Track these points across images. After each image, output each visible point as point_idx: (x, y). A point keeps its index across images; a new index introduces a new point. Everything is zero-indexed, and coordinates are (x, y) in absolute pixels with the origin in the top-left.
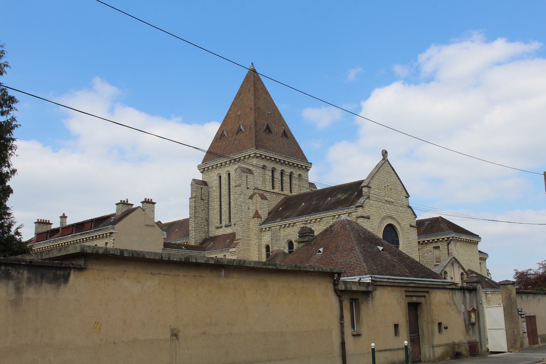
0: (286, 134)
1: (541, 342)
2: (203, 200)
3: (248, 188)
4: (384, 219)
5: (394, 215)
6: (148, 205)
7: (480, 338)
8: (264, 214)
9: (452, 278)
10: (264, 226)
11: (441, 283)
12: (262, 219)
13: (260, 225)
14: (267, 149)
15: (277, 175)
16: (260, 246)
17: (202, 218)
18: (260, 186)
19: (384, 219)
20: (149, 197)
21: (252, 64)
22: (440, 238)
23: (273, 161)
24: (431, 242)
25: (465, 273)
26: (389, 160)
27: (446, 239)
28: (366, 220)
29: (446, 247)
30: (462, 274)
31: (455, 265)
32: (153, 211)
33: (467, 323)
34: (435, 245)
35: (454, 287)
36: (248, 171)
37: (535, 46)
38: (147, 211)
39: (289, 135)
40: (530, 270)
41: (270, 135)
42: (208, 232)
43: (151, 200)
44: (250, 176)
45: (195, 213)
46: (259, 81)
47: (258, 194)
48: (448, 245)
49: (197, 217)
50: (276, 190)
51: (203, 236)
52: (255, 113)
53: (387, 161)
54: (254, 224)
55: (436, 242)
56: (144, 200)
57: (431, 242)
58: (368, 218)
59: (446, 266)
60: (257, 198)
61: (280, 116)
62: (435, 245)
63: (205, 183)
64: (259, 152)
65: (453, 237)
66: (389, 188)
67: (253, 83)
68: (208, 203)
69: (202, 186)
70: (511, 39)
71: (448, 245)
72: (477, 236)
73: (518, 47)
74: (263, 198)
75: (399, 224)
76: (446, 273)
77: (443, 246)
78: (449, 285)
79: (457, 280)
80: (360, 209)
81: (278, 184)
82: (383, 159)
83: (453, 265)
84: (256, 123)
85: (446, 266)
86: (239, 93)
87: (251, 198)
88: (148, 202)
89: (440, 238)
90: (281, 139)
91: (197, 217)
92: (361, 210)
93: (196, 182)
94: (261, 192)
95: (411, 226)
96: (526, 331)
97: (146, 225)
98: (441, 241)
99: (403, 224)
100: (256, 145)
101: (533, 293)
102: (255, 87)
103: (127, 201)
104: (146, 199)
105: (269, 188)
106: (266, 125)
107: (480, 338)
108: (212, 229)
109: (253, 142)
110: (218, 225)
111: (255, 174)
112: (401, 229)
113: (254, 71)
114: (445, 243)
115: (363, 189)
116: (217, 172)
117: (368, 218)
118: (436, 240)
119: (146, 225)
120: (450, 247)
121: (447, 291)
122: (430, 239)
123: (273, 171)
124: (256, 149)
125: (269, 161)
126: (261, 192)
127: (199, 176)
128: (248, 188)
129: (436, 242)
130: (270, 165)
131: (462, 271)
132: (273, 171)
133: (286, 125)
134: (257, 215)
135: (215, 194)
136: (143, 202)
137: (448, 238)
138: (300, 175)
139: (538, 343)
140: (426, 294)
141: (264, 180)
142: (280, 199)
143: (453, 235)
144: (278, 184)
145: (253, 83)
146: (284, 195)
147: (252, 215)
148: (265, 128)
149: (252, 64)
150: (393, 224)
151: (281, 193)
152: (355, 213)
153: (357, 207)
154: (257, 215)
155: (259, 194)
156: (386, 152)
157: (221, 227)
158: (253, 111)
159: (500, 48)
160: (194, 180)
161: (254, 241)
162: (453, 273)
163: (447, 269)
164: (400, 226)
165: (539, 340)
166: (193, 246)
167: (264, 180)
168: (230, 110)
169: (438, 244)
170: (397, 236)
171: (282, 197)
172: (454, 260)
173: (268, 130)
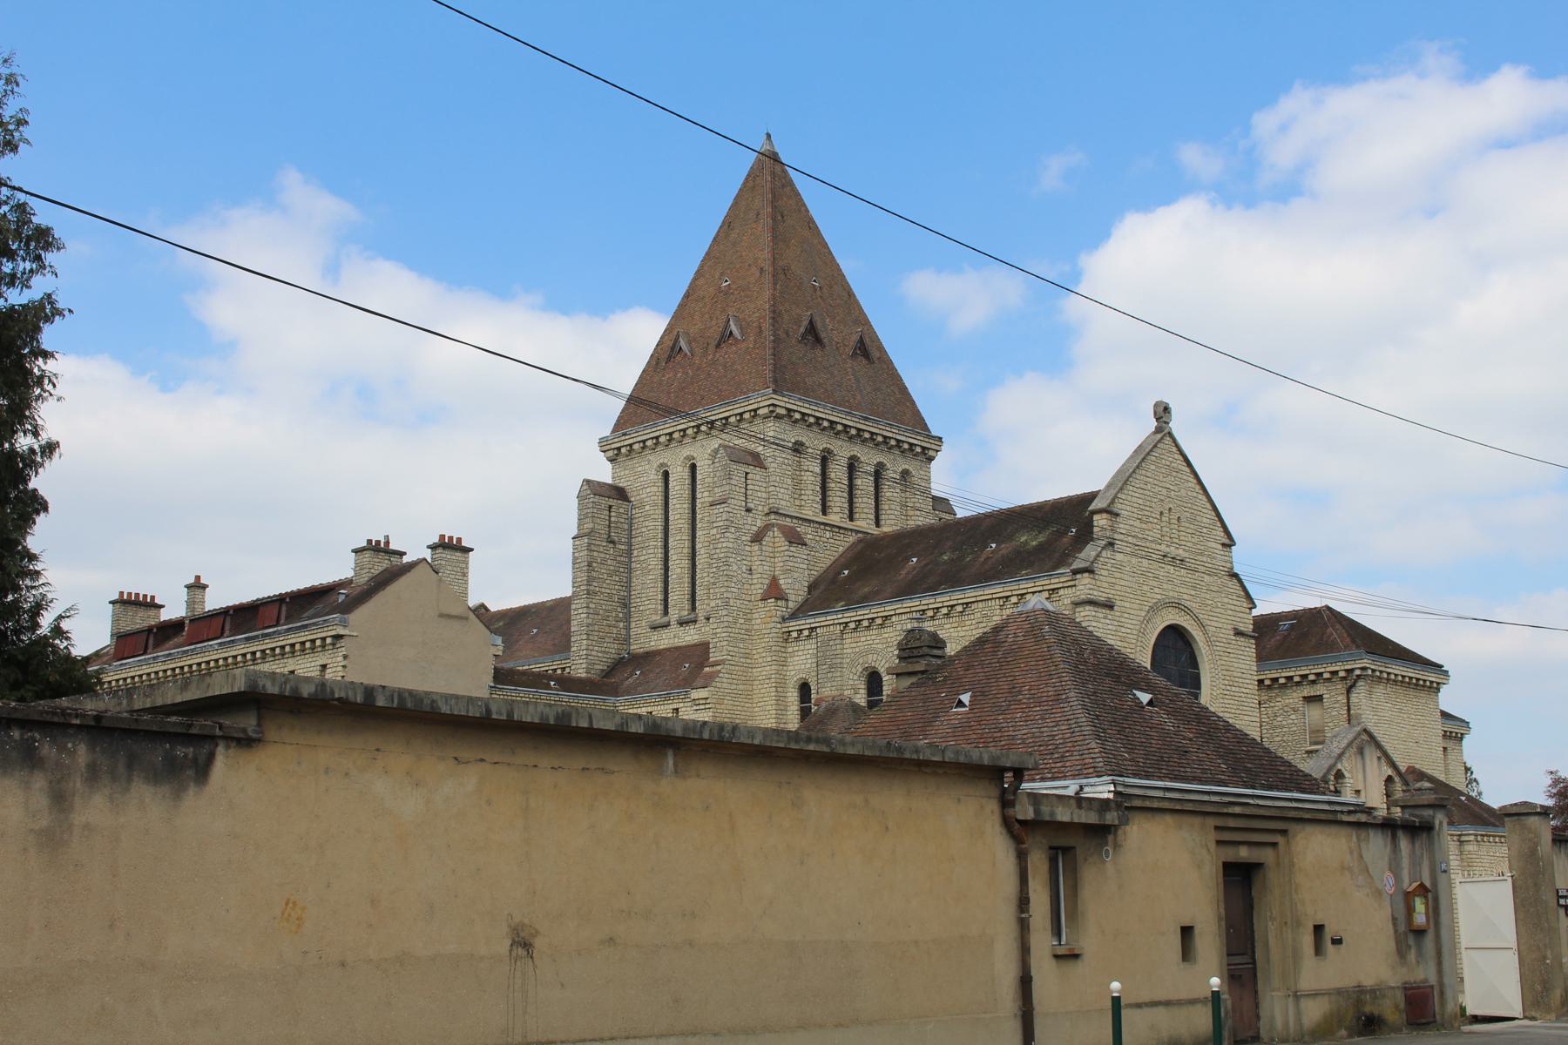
0: (867, 350)
2: (613, 542)
3: (748, 510)
4: (1155, 609)
6: (448, 555)
9: (1358, 792)
10: (794, 625)
11: (1327, 807)
12: (791, 604)
14: (805, 392)
15: (838, 472)
16: (780, 685)
18: (785, 505)
19: (1155, 609)
20: (453, 532)
21: (769, 136)
22: (1325, 669)
23: (824, 429)
24: (1298, 684)
25: (1397, 779)
27: (1342, 674)
29: (1343, 699)
30: (1389, 780)
32: (465, 575)
35: (1363, 818)
36: (749, 459)
39: (875, 354)
41: (818, 352)
42: (627, 639)
43: (459, 540)
44: (756, 474)
45: (589, 582)
48: (1349, 691)
49: (595, 593)
50: (834, 518)
51: (612, 650)
53: (1170, 434)
54: (766, 617)
55: (1313, 682)
57: (1298, 684)
59: (1340, 756)
60: (776, 539)
64: (784, 402)
66: (1174, 517)
67: (771, 192)
68: (630, 552)
69: (612, 502)
71: (1349, 691)
72: (1437, 667)
74: (795, 539)
75: (1202, 626)
76: (1339, 775)
77: (1333, 695)
78: (1350, 812)
79: (1375, 798)
80: (1085, 579)
81: (838, 500)
82: (1158, 430)
83: (1361, 751)
84: (776, 316)
85: (1340, 756)
86: (728, 225)
87: (757, 538)
88: (450, 547)
89: (1325, 669)
91: (595, 593)
92: (1086, 581)
93: (592, 489)
95: (1238, 633)
97: (441, 616)
99: (1212, 625)
100: (775, 381)
102: (774, 207)
103: (387, 543)
105: (812, 510)
106: (805, 323)
109: (768, 371)
110: (658, 618)
112: (1209, 642)
113: (774, 158)
114: (1341, 687)
119: (441, 616)
120: (1354, 698)
121: (1344, 831)
124: (775, 392)
125: (815, 428)
127: (604, 473)
128: (748, 510)
129: (1313, 682)
130: (816, 442)
133: (867, 323)
134: (774, 591)
135: (649, 526)
136: (433, 547)
138: (905, 474)
140: (1279, 839)
141: (798, 485)
143: (1365, 663)
144: (838, 500)
145: (771, 192)
146: (857, 532)
148: (802, 330)
149: (769, 136)
150: (1189, 628)
151: (849, 525)
153: (1075, 572)
154: (774, 591)
156: (1166, 409)
157: (667, 625)
158: (768, 278)
159: (1509, 95)
160: (588, 482)
161: (764, 669)
162: (1360, 776)
163: (1344, 766)
164: (1205, 633)
166: (580, 680)
167: (798, 485)
170: (1194, 663)
171: (852, 538)
172: (1365, 737)
173: (813, 334)
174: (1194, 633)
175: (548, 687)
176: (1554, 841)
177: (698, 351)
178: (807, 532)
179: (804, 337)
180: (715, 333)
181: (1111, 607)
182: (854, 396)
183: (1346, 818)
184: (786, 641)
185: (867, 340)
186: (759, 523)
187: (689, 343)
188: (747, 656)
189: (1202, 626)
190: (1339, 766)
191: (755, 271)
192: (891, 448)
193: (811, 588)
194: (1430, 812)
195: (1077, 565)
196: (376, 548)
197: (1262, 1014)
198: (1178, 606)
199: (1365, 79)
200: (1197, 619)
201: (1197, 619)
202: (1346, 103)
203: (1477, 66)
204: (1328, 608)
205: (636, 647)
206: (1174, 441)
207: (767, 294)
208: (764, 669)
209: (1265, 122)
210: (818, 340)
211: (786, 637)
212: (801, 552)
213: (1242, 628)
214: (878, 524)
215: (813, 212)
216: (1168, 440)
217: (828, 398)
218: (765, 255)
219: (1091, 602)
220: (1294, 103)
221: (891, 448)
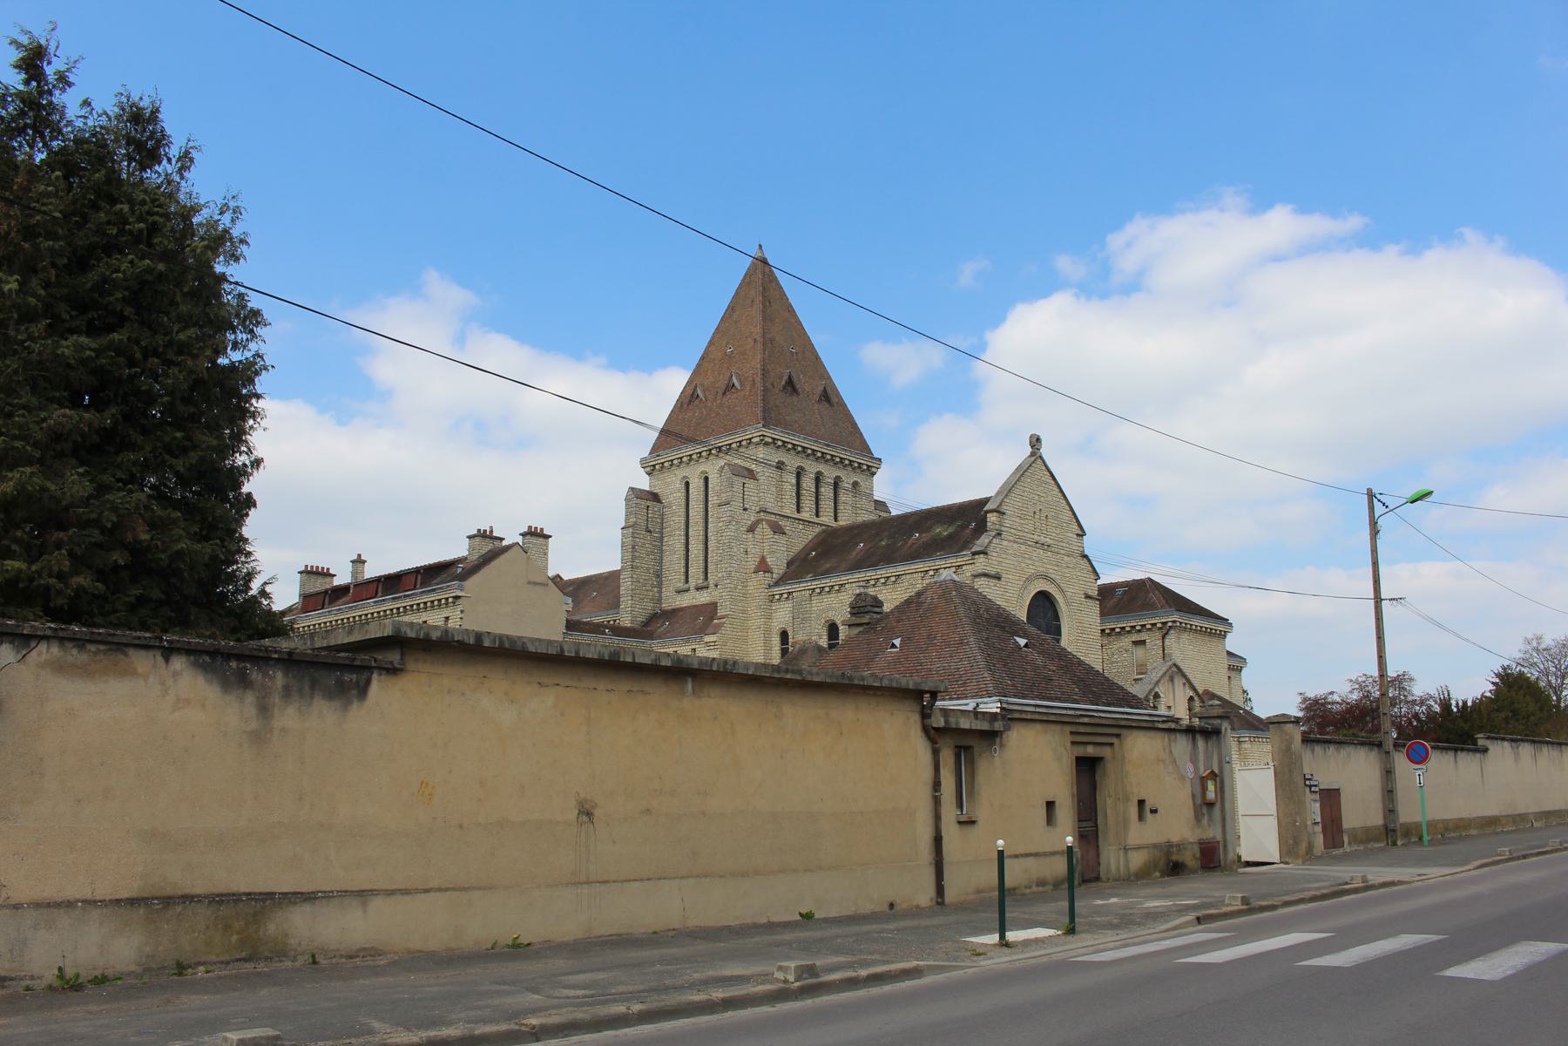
0: (829, 396)
4: (1030, 579)
6: (534, 540)
7: (1224, 832)
10: (777, 590)
15: (808, 483)
16: (767, 632)
18: (771, 507)
19: (1030, 579)
20: (537, 524)
22: (1148, 622)
29: (1159, 643)
30: (1191, 699)
33: (1199, 801)
34: (1135, 637)
35: (1173, 726)
38: (532, 552)
39: (834, 399)
41: (795, 398)
42: (660, 599)
44: (750, 484)
45: (634, 558)
50: (805, 515)
51: (649, 607)
59: (1157, 683)
60: (764, 529)
61: (817, 358)
62: (1135, 637)
64: (770, 433)
67: (761, 285)
68: (662, 538)
74: (778, 530)
77: (1153, 639)
79: (1181, 712)
80: (981, 559)
81: (808, 502)
82: (1032, 454)
83: (1172, 679)
84: (765, 373)
85: (1157, 683)
86: (731, 309)
87: (751, 529)
88: (535, 534)
89: (1148, 622)
93: (635, 493)
95: (1088, 597)
99: (1069, 590)
105: (790, 510)
107: (1224, 832)
110: (681, 585)
112: (1067, 603)
114: (1158, 635)
116: (681, 473)
117: (998, 577)
121: (1159, 735)
122: (1127, 625)
127: (644, 482)
130: (793, 462)
134: (763, 567)
135: (675, 520)
137: (1164, 624)
138: (855, 484)
140: (1114, 740)
143: (1175, 618)
144: (808, 502)
145: (761, 285)
147: (752, 566)
151: (797, 516)
153: (974, 554)
154: (763, 567)
155: (770, 523)
156: (1038, 440)
161: (756, 621)
163: (1160, 689)
165: (1346, 839)
166: (627, 629)
167: (780, 494)
168: (711, 343)
170: (1057, 618)
171: (818, 530)
181: (999, 579)
193: (789, 564)
195: (975, 549)
196: (484, 535)
198: (1046, 578)
200: (1059, 587)
201: (1059, 587)
208: (756, 621)
210: (795, 390)
211: (771, 599)
219: (985, 575)
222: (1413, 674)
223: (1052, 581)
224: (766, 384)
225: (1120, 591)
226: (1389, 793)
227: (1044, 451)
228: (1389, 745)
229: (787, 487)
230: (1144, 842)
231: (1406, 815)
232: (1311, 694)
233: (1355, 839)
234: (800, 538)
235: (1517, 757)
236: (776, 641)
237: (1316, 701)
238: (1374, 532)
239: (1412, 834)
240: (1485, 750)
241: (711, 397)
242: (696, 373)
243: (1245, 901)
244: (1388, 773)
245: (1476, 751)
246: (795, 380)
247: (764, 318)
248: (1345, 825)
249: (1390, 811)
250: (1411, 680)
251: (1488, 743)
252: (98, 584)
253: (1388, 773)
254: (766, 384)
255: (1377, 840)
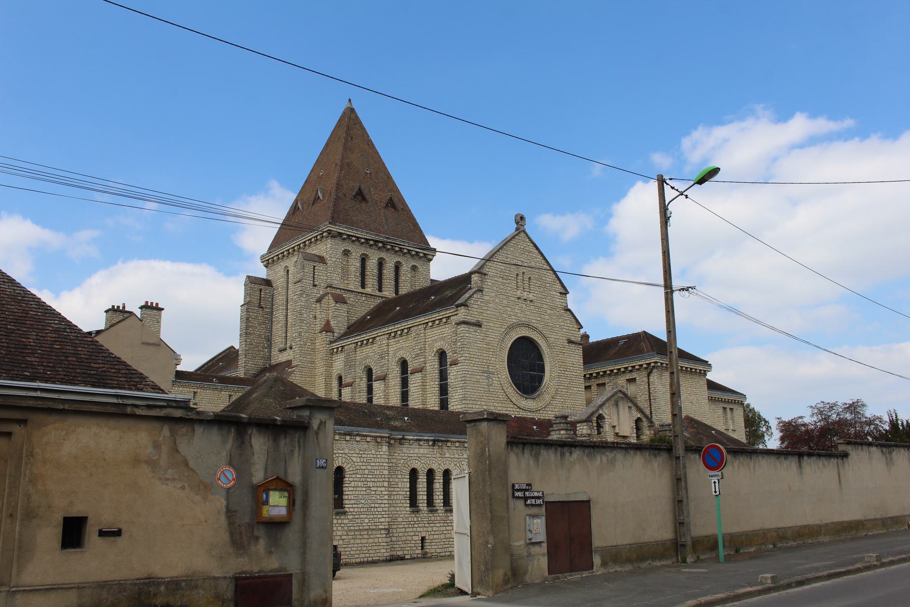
0: (395, 203)
1: (604, 564)
2: (262, 308)
3: (315, 286)
4: (512, 327)
5: (534, 322)
6: (148, 312)
7: (304, 561)
8: (339, 327)
9: (614, 427)
10: (335, 345)
11: (114, 401)
12: (336, 335)
13: (331, 342)
14: (351, 224)
15: (372, 264)
16: (328, 377)
17: (260, 336)
18: (336, 283)
19: (512, 327)
20: (153, 300)
21: (350, 100)
22: (637, 364)
23: (362, 243)
24: (624, 372)
25: (644, 419)
26: (527, 231)
27: (645, 366)
28: (472, 329)
29: (645, 379)
30: (638, 421)
31: (621, 404)
32: (159, 322)
33: (245, 518)
34: (629, 376)
35: (178, 413)
36: (317, 259)
37: (849, 123)
38: (147, 322)
39: (400, 206)
40: (801, 417)
41: (363, 205)
42: (270, 358)
43: (157, 304)
44: (320, 267)
45: (247, 328)
46: (357, 126)
47: (333, 294)
48: (649, 375)
49: (251, 334)
50: (368, 290)
51: (261, 363)
52: (341, 170)
53: (524, 231)
54: (321, 341)
55: (631, 371)
56: (143, 304)
57: (624, 372)
58: (478, 325)
59: (601, 406)
60: (329, 300)
61: (389, 176)
62: (629, 376)
63: (268, 283)
64: (335, 229)
65: (656, 362)
66: (526, 278)
67: (350, 128)
68: (272, 313)
69: (261, 287)
70: (813, 114)
71: (649, 375)
72: (705, 363)
73: (822, 125)
74: (340, 300)
75: (545, 337)
76: (601, 418)
77: (641, 377)
78: (149, 407)
79: (627, 428)
80: (462, 310)
81: (371, 281)
82: (517, 229)
83: (616, 404)
84: (339, 186)
85: (601, 406)
86: (327, 145)
87: (319, 300)
88: (152, 308)
89: (637, 364)
90: (383, 210)
91: (251, 334)
92: (463, 311)
93: (252, 281)
94: (338, 292)
95: (570, 342)
96: (542, 536)
97: (143, 343)
98: (638, 369)
99: (552, 337)
100: (333, 218)
101: (824, 456)
102: (347, 134)
103: (124, 307)
104: (147, 302)
105: (354, 285)
106: (357, 189)
107: (304, 561)
108: (275, 352)
109: (329, 213)
110: (282, 346)
111: (329, 263)
112: (549, 346)
113: (352, 110)
114: (645, 373)
115: (473, 276)
116: (283, 264)
117: (478, 325)
118: (630, 369)
119: (143, 343)
120: (651, 380)
121: (144, 425)
122: (622, 366)
123: (364, 260)
124: (330, 223)
125: (357, 243)
126: (338, 292)
127: (261, 272)
128: (315, 286)
129: (631, 371)
130: (357, 252)
131: (639, 415)
132: (364, 260)
133: (398, 191)
134: (327, 328)
135: (280, 299)
136: (141, 308)
137: (649, 364)
138: (414, 268)
139: (590, 566)
140: (16, 429)
141: (345, 273)
142: (373, 304)
143: (656, 359)
144: (371, 281)
145: (350, 128)
146: (382, 297)
147: (318, 328)
148: (354, 193)
149: (350, 100)
150: (536, 339)
151: (378, 293)
152: (455, 317)
153: (458, 306)
154: (327, 328)
155: (333, 294)
156: (522, 218)
157: (285, 350)
158: (338, 168)
159: (799, 126)
160: (248, 277)
161: (320, 370)
162: (615, 418)
163: (604, 412)
164: (547, 341)
165: (597, 560)
166: (241, 379)
167: (345, 273)
168: (312, 171)
169: (634, 375)
170: (540, 357)
171: (379, 301)
172: (620, 395)
173: (360, 195)
174: (539, 342)
175: (212, 381)
176: (508, 443)
177: (305, 208)
178: (350, 298)
179: (355, 197)
180: (312, 198)
181: (480, 326)
182: (383, 227)
183: (139, 412)
184: (332, 354)
185: (395, 200)
186: (321, 293)
187: (302, 204)
188: (313, 362)
189: (545, 337)
190: (601, 412)
191: (334, 165)
192: (404, 254)
193: (348, 328)
194: (306, 413)
195: (459, 302)
196: (113, 310)
197: (873, 517)
198: (528, 326)
199: (731, 122)
200: (541, 333)
201: (541, 333)
202: (720, 132)
203: (783, 116)
204: (644, 332)
205: (273, 362)
206: (527, 235)
207: (336, 175)
208: (320, 370)
209: (686, 143)
210: (364, 199)
211: (332, 353)
212: (344, 308)
213: (573, 339)
214: (380, 290)
215: (371, 137)
216: (522, 234)
217: (366, 227)
218: (338, 157)
219: (464, 323)
220: (698, 134)
221: (404, 254)
222: (865, 401)
223: (535, 329)
224: (352, 196)
225: (622, 342)
226: (679, 503)
227: (527, 228)
228: (680, 450)
229: (352, 269)
230: (76, 579)
231: (702, 525)
232: (786, 419)
233: (614, 556)
234: (362, 308)
235: (889, 463)
236: (335, 383)
237: (790, 423)
238: (665, 218)
239: (707, 545)
240: (845, 455)
241: (305, 208)
242: (301, 192)
243: (878, 558)
244: (679, 482)
245: (830, 456)
246: (365, 192)
247: (345, 149)
248: (597, 542)
249: (680, 524)
250: (863, 405)
251: (848, 449)
252: (777, 434)
253: (679, 482)
254: (352, 196)
255: (662, 557)
